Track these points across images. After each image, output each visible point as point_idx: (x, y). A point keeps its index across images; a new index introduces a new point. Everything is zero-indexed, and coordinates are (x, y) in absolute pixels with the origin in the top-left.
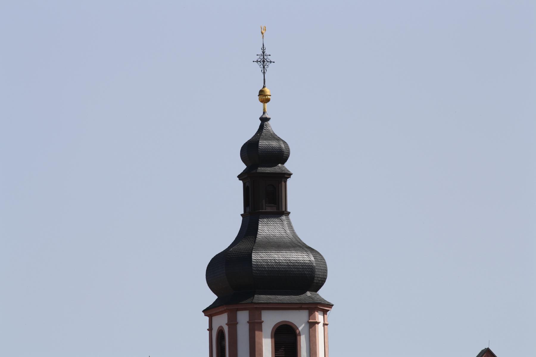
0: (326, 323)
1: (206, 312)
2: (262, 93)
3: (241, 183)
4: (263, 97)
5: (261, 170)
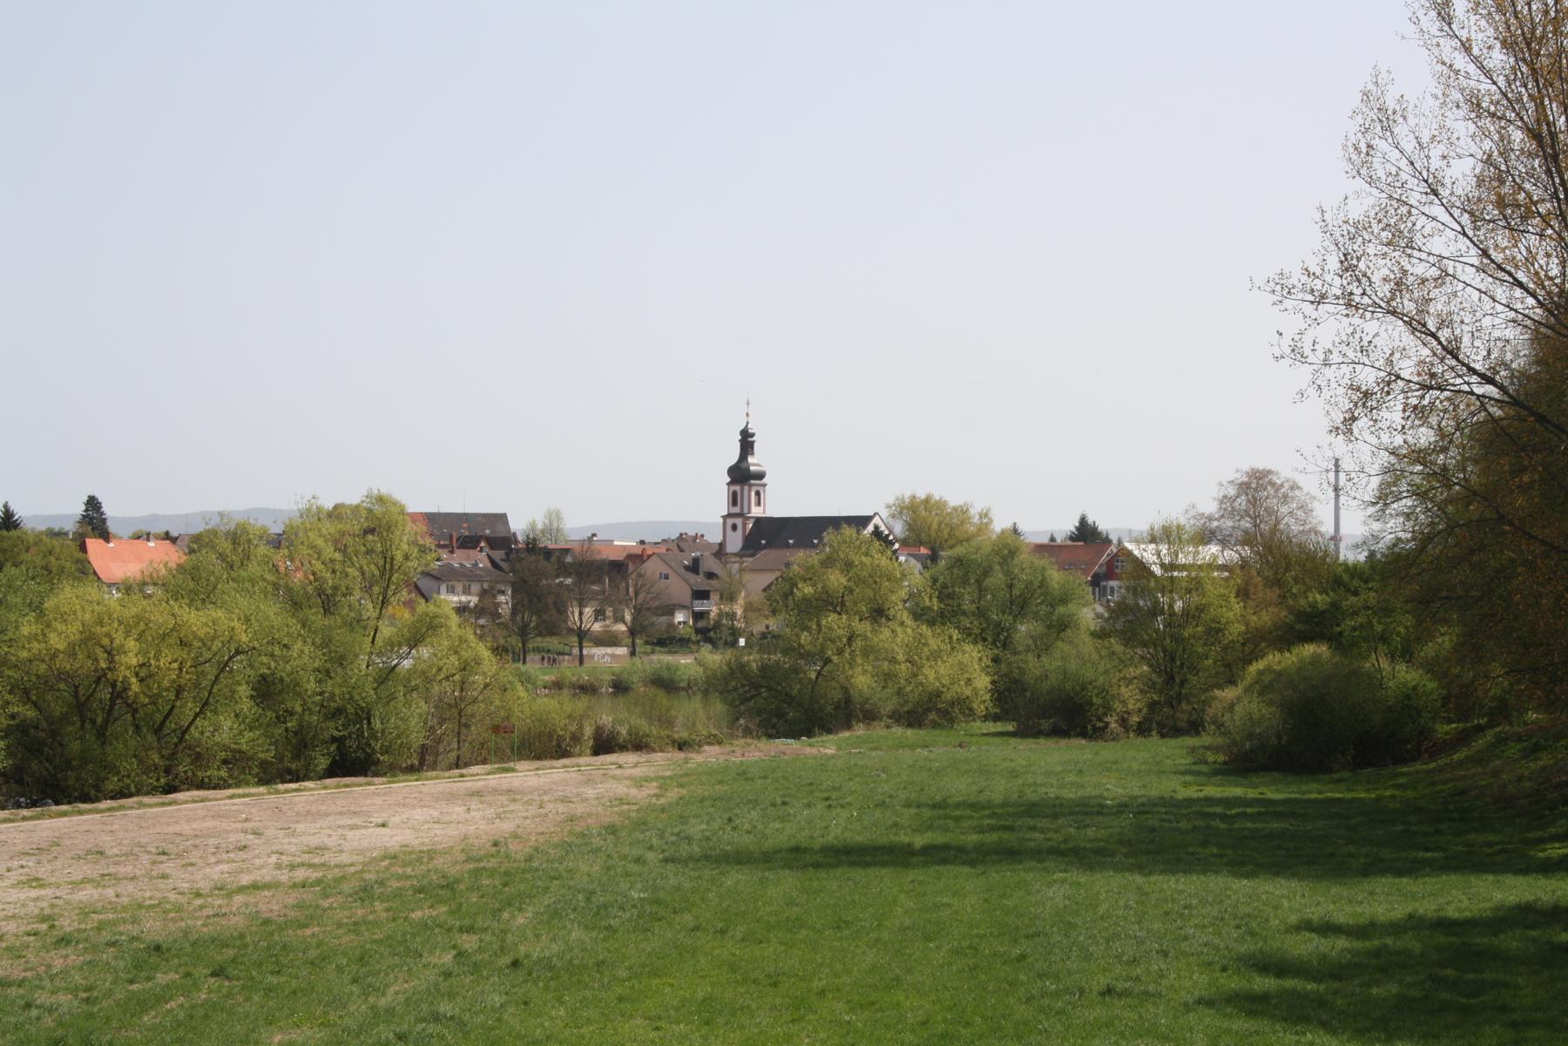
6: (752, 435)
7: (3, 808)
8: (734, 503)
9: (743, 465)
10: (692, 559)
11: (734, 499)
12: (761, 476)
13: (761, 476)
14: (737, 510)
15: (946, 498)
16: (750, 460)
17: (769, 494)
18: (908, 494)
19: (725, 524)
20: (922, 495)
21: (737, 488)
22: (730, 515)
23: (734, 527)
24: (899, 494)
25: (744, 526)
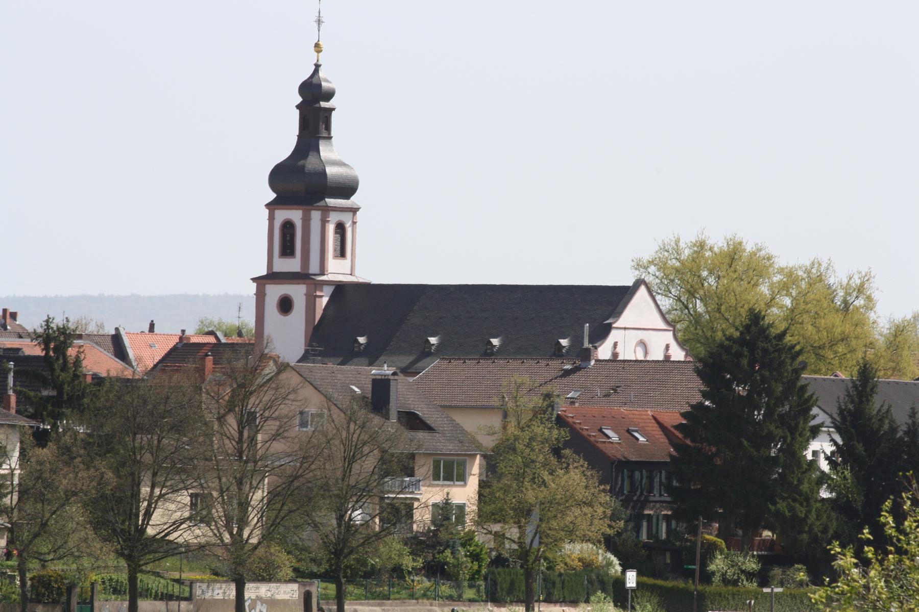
0: (146, 328)
1: (268, 206)
2: (317, 45)
3: (298, 111)
4: (318, 47)
5: (645, 524)
6: (329, 95)
7: (533, 610)
8: (287, 250)
9: (310, 163)
10: (212, 363)
11: (286, 240)
12: (347, 189)
13: (347, 189)
14: (292, 265)
15: (771, 249)
16: (326, 152)
17: (365, 233)
18: (688, 238)
19: (260, 296)
20: (717, 241)
21: (295, 215)
22: (272, 277)
23: (285, 305)
24: (668, 237)
25: (311, 301)
